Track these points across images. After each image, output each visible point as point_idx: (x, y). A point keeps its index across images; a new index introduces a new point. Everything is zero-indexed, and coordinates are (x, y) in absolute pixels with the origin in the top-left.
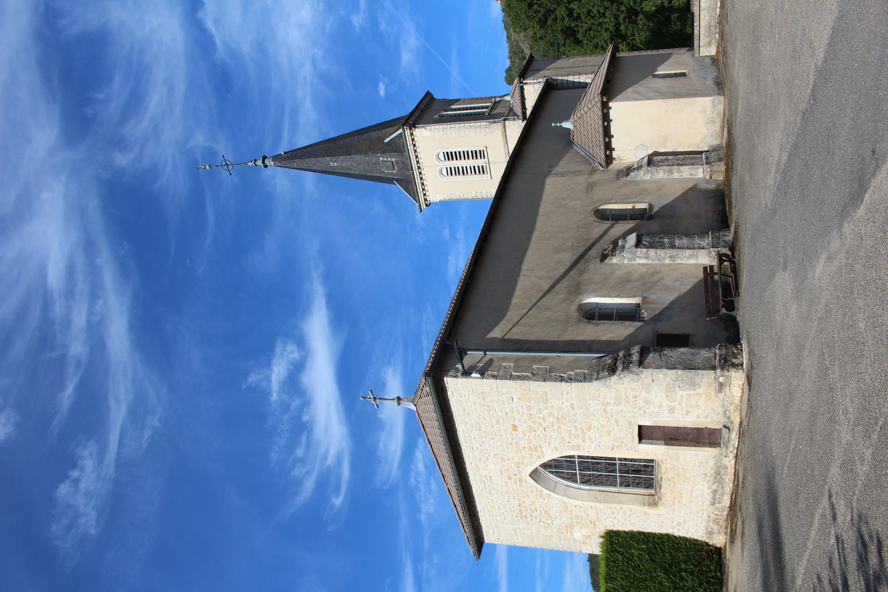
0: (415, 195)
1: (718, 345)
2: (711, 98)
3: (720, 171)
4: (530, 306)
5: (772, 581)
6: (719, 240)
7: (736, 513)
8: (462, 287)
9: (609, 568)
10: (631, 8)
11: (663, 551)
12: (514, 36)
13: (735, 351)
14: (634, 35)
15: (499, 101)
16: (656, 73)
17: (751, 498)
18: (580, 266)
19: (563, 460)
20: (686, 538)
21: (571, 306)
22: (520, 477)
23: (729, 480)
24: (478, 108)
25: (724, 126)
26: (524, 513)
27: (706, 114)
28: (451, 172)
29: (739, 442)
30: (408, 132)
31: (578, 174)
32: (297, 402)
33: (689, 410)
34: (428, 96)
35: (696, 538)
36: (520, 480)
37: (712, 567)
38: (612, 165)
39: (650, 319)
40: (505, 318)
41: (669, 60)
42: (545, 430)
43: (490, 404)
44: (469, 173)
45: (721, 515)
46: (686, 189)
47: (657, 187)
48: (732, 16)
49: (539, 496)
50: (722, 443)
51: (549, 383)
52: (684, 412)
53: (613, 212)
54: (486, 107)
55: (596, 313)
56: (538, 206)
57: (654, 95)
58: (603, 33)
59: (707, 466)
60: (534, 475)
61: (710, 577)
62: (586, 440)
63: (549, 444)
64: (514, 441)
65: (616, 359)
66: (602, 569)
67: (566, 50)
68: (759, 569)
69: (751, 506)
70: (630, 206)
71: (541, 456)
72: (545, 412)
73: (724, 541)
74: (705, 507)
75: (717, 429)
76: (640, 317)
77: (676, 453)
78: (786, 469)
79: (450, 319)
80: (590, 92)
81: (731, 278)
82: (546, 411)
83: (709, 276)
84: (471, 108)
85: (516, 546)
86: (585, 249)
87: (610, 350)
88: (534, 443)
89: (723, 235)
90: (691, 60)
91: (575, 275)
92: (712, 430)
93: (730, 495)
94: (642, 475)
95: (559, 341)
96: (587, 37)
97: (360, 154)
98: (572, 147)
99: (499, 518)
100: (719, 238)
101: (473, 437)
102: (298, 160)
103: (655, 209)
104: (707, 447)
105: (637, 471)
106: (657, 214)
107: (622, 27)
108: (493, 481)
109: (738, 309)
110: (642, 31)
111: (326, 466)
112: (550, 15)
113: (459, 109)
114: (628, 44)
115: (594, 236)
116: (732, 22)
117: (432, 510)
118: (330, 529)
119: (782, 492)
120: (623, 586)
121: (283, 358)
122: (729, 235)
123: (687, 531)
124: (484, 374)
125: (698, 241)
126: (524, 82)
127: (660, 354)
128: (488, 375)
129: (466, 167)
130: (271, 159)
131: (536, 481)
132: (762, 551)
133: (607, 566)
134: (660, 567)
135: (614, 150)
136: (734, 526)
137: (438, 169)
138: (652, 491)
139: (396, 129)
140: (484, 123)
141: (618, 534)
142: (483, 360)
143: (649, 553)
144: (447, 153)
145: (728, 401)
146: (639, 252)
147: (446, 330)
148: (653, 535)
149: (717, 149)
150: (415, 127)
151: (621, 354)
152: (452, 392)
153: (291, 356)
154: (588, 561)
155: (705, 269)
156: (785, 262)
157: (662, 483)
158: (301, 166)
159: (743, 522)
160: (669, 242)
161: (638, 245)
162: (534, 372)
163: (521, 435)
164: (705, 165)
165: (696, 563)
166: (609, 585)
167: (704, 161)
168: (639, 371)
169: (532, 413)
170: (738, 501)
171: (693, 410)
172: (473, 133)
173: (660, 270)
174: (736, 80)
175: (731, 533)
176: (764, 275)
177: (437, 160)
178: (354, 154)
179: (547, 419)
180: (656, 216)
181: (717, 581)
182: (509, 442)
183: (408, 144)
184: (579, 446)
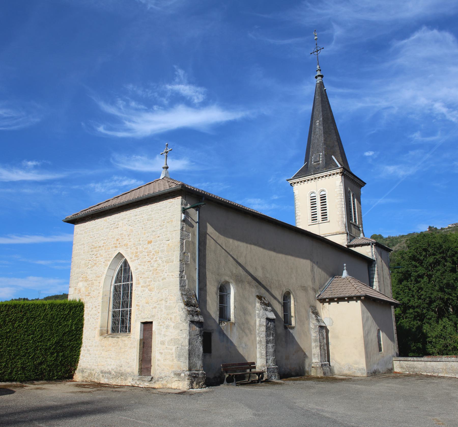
0: (297, 176)
1: (205, 372)
2: (365, 368)
4: (228, 251)
5: (51, 412)
6: (272, 373)
7: (96, 387)
8: (239, 207)
9: (59, 306)
10: (425, 317)
11: (70, 341)
12: (404, 240)
14: (406, 318)
15: (359, 230)
16: (381, 332)
17: (106, 397)
18: (254, 282)
19: (129, 274)
22: (118, 247)
23: (117, 382)
24: (355, 216)
25: (347, 376)
26: (94, 250)
27: (354, 364)
28: (313, 199)
29: (142, 387)
30: (339, 171)
31: (313, 281)
32: (166, 102)
33: (163, 354)
35: (79, 362)
36: (116, 247)
37: (60, 373)
39: (221, 328)
40: (220, 235)
41: (390, 341)
42: (149, 261)
43: (164, 226)
44: (312, 211)
45: (94, 378)
46: (305, 351)
47: (306, 332)
48: (421, 383)
49: (106, 259)
50: (141, 376)
51: (179, 263)
52: (161, 351)
53: (289, 303)
54: (355, 222)
55: (223, 293)
56: (292, 255)
58: (407, 298)
59: (126, 367)
60: (120, 255)
61: (53, 372)
62: (143, 288)
63: (140, 264)
64: (141, 242)
65: (195, 306)
66: (59, 301)
67: (395, 274)
68: (59, 403)
69: (100, 397)
70: (293, 314)
71: (132, 259)
72: (160, 261)
73: (77, 380)
74: (100, 367)
75: (151, 373)
76: (222, 321)
77: (135, 347)
78: (125, 418)
79: (219, 200)
80: (367, 288)
81: (248, 380)
82: (161, 262)
83: (249, 366)
84: (355, 212)
85: (73, 245)
86: (265, 285)
87: (200, 302)
89: (275, 375)
90: (390, 355)
92: (150, 369)
93: (108, 383)
94: (121, 325)
95: (206, 270)
96: (404, 287)
97: (324, 140)
98: (330, 276)
99: (91, 233)
102: (320, 99)
103: (291, 331)
104: (139, 367)
105: (123, 322)
106: (288, 332)
107: (411, 311)
108: (115, 229)
109: (228, 385)
110: (410, 324)
112: (418, 263)
113: (354, 204)
114: (400, 314)
116: (417, 382)
117: (97, 190)
118: (83, 124)
119: (110, 416)
120: (47, 316)
121: (194, 92)
123: (84, 356)
124: (184, 222)
125: (271, 358)
126: (373, 246)
127: (198, 335)
128: (183, 224)
129: (316, 209)
130: (321, 81)
131: (115, 257)
132: (71, 404)
133: (61, 305)
134: (60, 339)
136: (87, 386)
137: (315, 191)
138: (110, 332)
139: (341, 163)
140: (345, 220)
142: (193, 221)
143: (69, 332)
144: (325, 197)
145: (169, 379)
146: (263, 320)
147: (211, 197)
148: (81, 334)
150: (342, 176)
152: (172, 202)
153: (195, 98)
154: (64, 294)
155: (254, 363)
156: (259, 415)
158: (316, 101)
159: (90, 392)
160: (270, 339)
161: (268, 319)
163: (145, 246)
164: (321, 363)
165: (63, 362)
166: (48, 306)
167: (323, 363)
168: (187, 321)
169: (160, 253)
170: (104, 389)
171: (163, 357)
172: (338, 213)
174: (377, 384)
175: (82, 384)
176: (250, 401)
178: (324, 136)
179: (156, 263)
180: (287, 331)
181: (51, 376)
182: (140, 239)
183: (331, 171)
184: (139, 284)
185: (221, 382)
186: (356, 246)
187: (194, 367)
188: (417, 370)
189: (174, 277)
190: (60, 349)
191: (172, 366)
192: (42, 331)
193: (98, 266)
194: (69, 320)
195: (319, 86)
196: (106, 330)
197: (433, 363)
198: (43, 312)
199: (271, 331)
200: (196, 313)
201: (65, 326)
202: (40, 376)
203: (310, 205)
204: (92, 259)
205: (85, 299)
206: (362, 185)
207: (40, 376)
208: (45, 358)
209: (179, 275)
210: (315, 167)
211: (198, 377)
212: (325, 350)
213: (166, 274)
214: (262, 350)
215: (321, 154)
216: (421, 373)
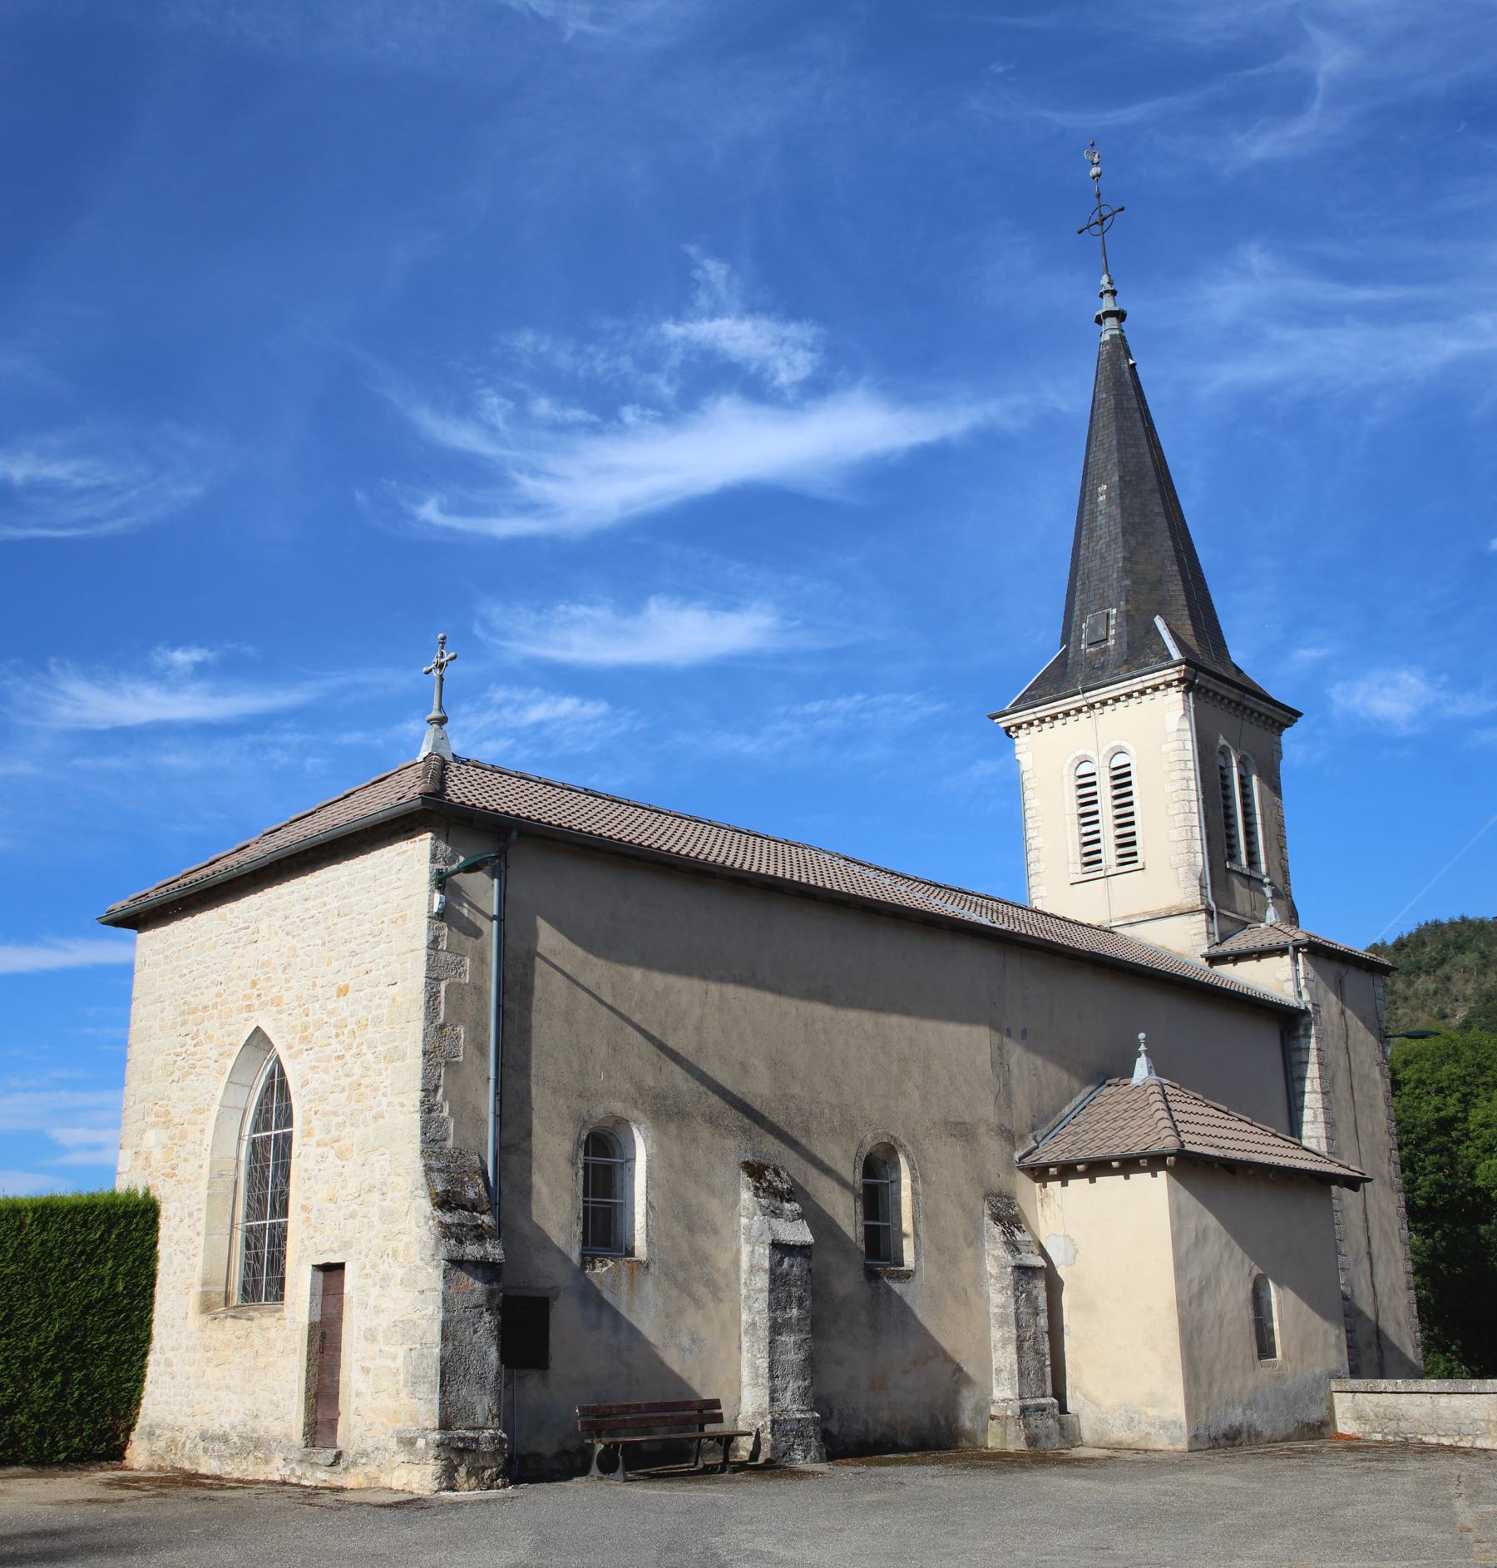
1: (504, 1435)
2: (1184, 1419)
3: (1006, 1440)
9: (69, 1212)
13: (487, 1473)
18: (733, 1117)
20: (143, 1381)
21: (623, 1102)
22: (256, 1007)
26: (190, 1018)
28: (1086, 783)
30: (1172, 674)
32: (666, 391)
34: (1285, 713)
36: (249, 1008)
37: (77, 1440)
38: (1030, 1181)
39: (589, 1283)
40: (591, 957)
42: (338, 1057)
46: (958, 1358)
49: (222, 1050)
52: (366, 1364)
54: (1253, 862)
56: (905, 1012)
57: (1192, 1281)
59: (271, 1419)
60: (259, 1039)
61: (53, 1438)
63: (314, 1067)
64: (319, 991)
70: (907, 1226)
71: (292, 1051)
73: (136, 1466)
77: (295, 1349)
83: (696, 1412)
88: (316, 1034)
91: (709, 1106)
98: (1087, 1082)
100: (801, 1435)
101: (326, 899)
102: (1113, 402)
103: (896, 1287)
104: (307, 1417)
106: (882, 1290)
108: (249, 947)
111: (515, 476)
113: (1246, 796)
115: (818, 1144)
120: (26, 1247)
121: (773, 344)
122: (808, 1459)
123: (157, 1382)
126: (1300, 955)
127: (481, 1306)
128: (439, 928)
129: (1097, 822)
130: (1117, 332)
134: (72, 1325)
135: (1062, 1186)
137: (1092, 754)
138: (236, 1298)
140: (1200, 860)
141: (151, 1227)
143: (106, 1300)
144: (1128, 774)
146: (762, 1251)
148: (148, 1308)
149: (1066, 1434)
150: (1186, 692)
151: (486, 1219)
152: (406, 851)
153: (781, 364)
155: (716, 1404)
157: (243, 1322)
160: (790, 1318)
162: (448, 1029)
163: (330, 1006)
164: (1019, 1403)
165: (85, 1405)
166: (31, 1214)
167: (1029, 1402)
169: (370, 1028)
172: (1175, 835)
173: (721, 1300)
177: (1112, 749)
183: (1144, 678)
184: (309, 1134)
185: (584, 1471)
186: (1238, 957)
187: (464, 1416)
188: (1409, 1425)
189: (405, 1109)
190: (75, 1360)
191: (395, 1412)
192: (11, 1300)
193: (199, 1074)
194: (106, 1261)
195: (1108, 353)
196: (224, 1295)
197: (1458, 1401)
198: (15, 1236)
199: (794, 1289)
200: (474, 1233)
201: (90, 1280)
202: (10, 1452)
203: (1075, 806)
204: (184, 1049)
205: (163, 1186)
206: (1286, 721)
207: (10, 1452)
208: (23, 1389)
209: (418, 1104)
210: (1091, 662)
211: (474, 1451)
212: (1043, 1355)
213: (385, 1101)
214: (759, 1356)
215: (1114, 611)
216: (1419, 1437)
